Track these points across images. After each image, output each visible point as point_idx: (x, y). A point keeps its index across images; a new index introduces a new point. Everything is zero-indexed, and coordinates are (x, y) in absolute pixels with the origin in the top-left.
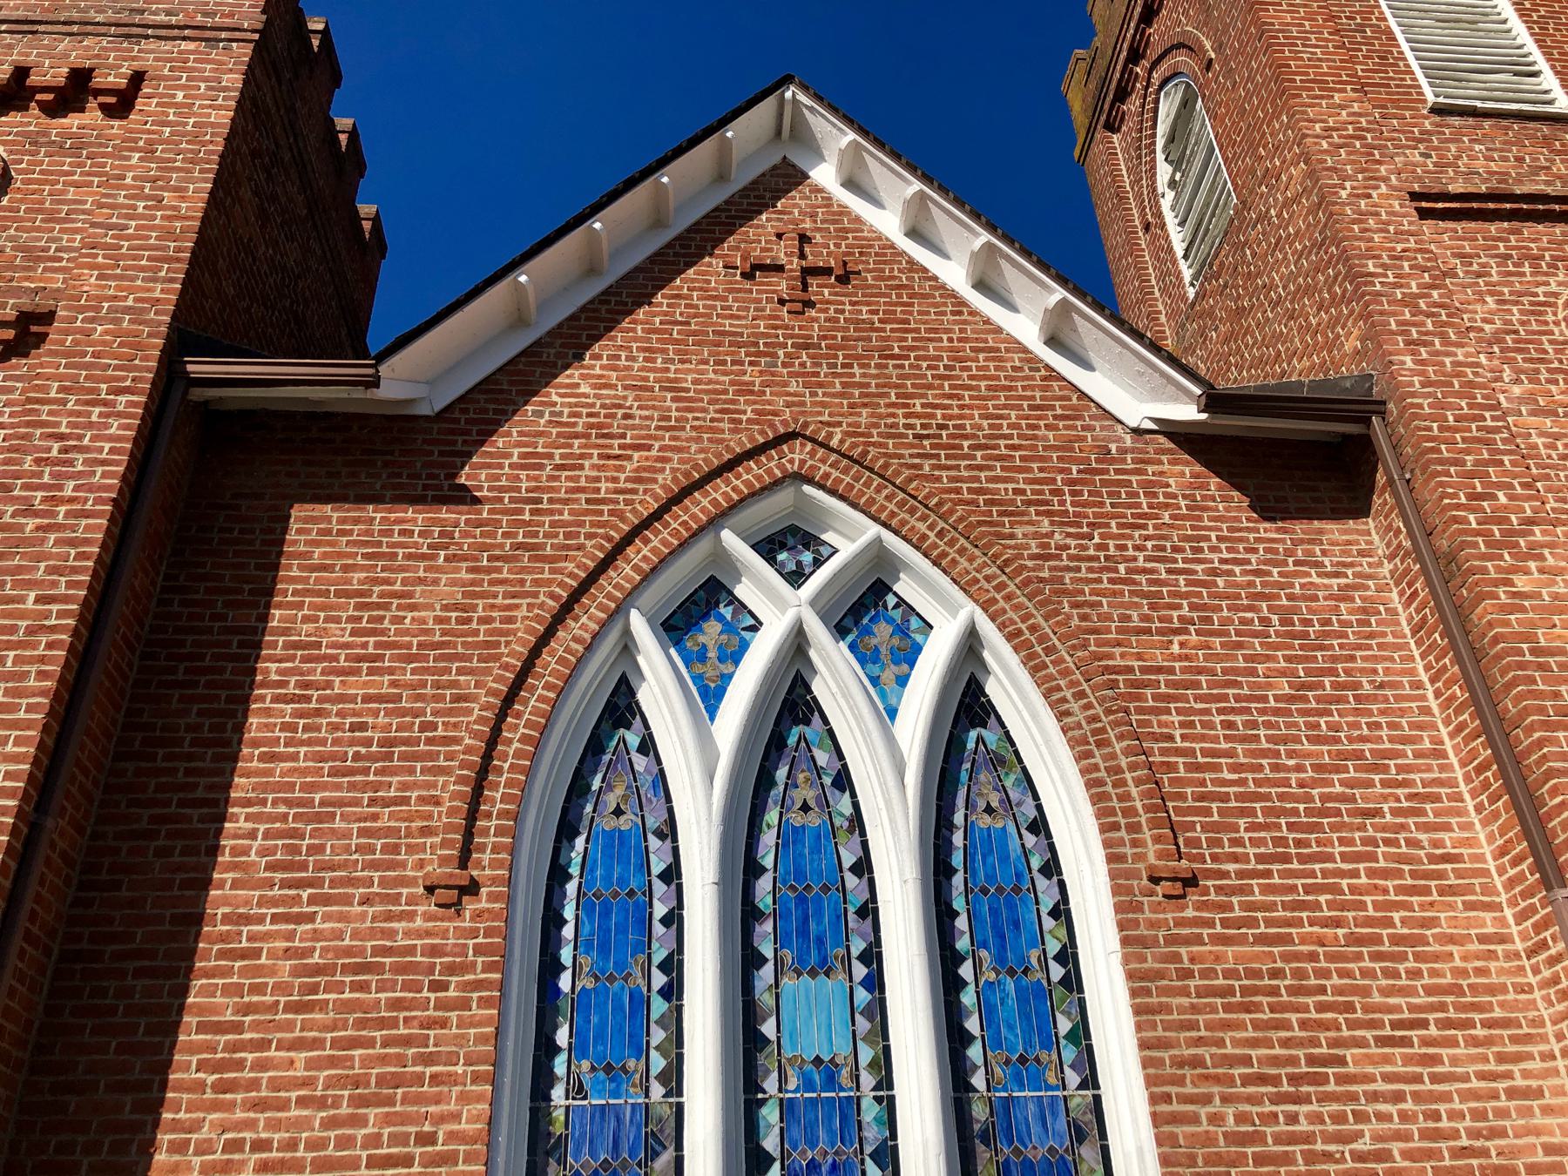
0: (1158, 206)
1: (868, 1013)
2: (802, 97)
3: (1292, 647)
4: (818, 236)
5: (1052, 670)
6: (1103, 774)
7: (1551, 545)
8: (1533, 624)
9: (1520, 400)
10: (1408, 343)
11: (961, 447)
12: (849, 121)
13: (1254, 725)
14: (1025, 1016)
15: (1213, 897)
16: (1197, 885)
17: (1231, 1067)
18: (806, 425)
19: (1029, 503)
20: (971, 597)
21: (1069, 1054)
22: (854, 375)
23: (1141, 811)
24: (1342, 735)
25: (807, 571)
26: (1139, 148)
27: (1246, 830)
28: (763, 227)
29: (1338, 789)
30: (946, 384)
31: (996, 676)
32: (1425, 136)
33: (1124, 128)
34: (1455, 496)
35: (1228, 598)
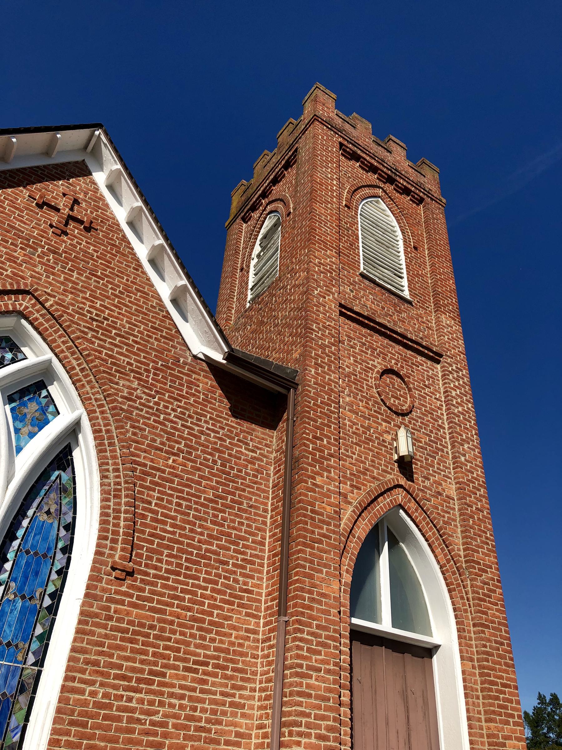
0: (249, 263)
2: (103, 137)
3: (221, 478)
4: (84, 204)
5: (108, 454)
6: (111, 511)
7: (335, 468)
8: (316, 499)
9: (348, 404)
10: (316, 364)
11: (111, 332)
12: (121, 159)
13: (190, 508)
14: (20, 621)
15: (138, 583)
16: (132, 576)
17: (112, 669)
18: (36, 290)
19: (132, 371)
20: (84, 405)
21: (35, 645)
22: (72, 276)
23: (121, 534)
24: (226, 523)
25: (6, 363)
26: (251, 234)
27: (166, 556)
28: (58, 186)
29: (214, 548)
30: (117, 299)
31: (81, 448)
32: (354, 284)
33: (249, 223)
34: (308, 434)
35: (203, 446)
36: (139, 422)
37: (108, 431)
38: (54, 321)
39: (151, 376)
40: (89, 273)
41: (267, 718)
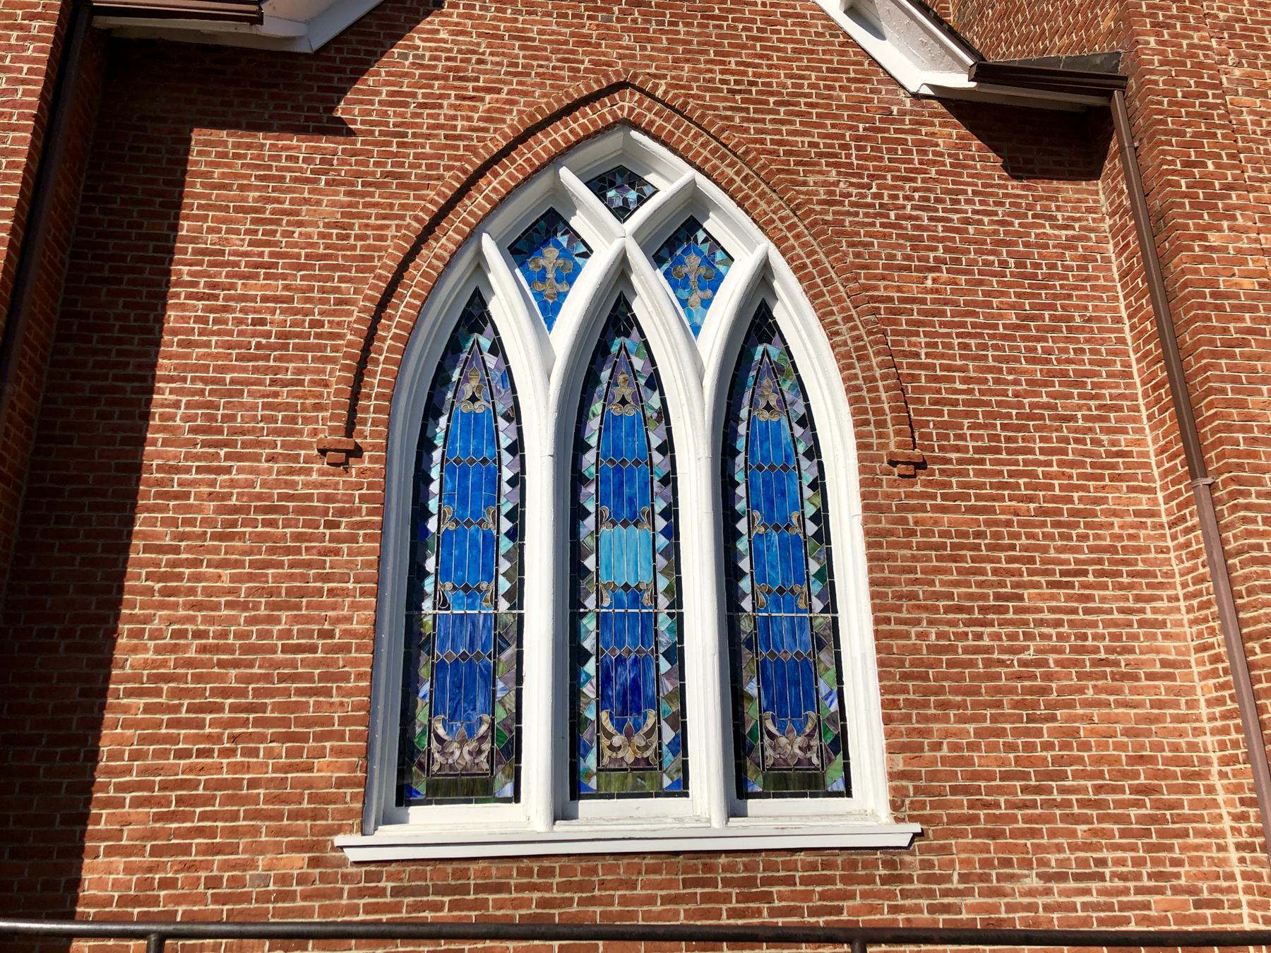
1: (666, 553)
3: (1023, 286)
5: (828, 298)
6: (860, 382)
7: (1242, 208)
9: (1240, 82)
10: (1154, 25)
11: (767, 103)
15: (937, 477)
16: (925, 468)
17: (938, 600)
18: (635, 76)
19: (821, 155)
20: (767, 234)
22: (678, 33)
25: (632, 207)
27: (969, 428)
29: (1045, 399)
30: (758, 45)
31: (782, 302)
35: (976, 243)
36: (858, 234)
37: (816, 263)
38: (677, 117)
39: (853, 152)
40: (702, 17)
41: (1212, 632)
